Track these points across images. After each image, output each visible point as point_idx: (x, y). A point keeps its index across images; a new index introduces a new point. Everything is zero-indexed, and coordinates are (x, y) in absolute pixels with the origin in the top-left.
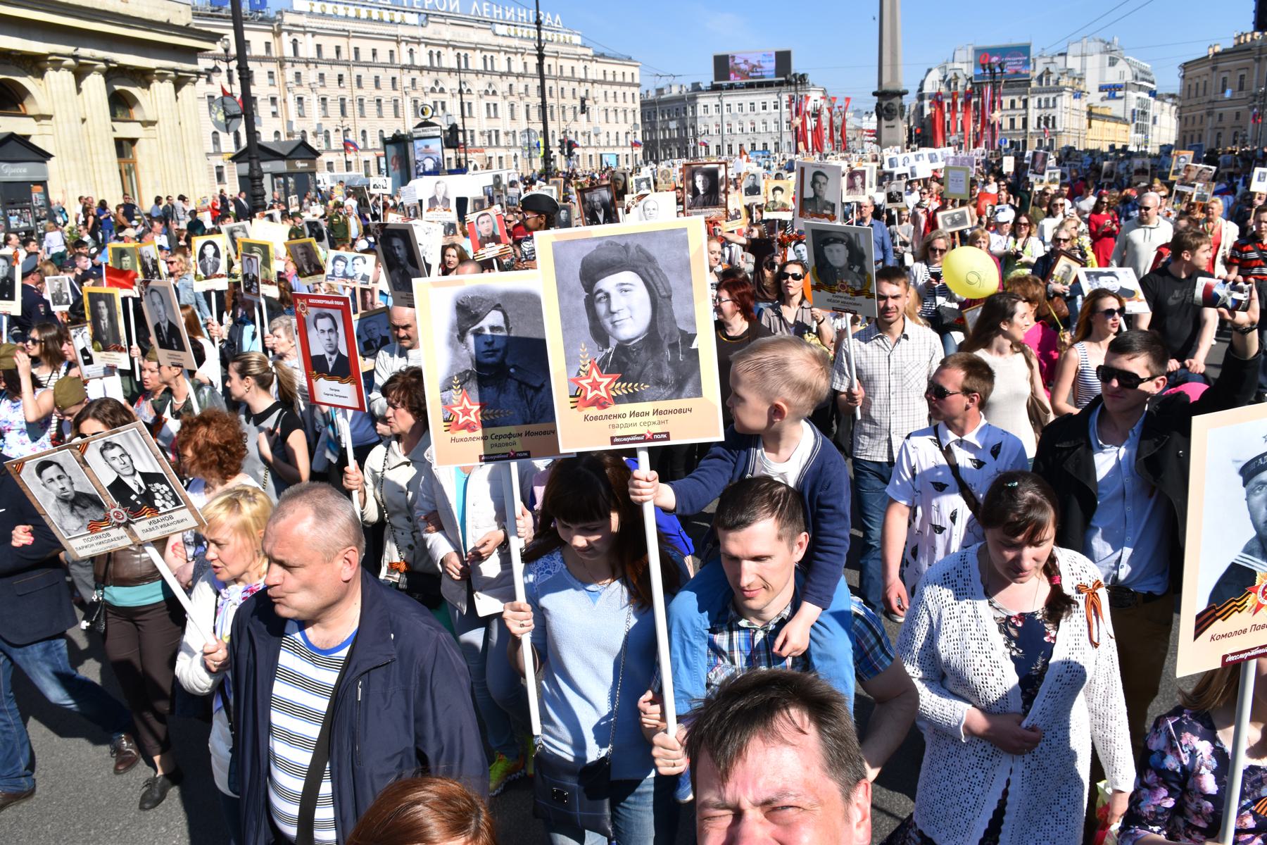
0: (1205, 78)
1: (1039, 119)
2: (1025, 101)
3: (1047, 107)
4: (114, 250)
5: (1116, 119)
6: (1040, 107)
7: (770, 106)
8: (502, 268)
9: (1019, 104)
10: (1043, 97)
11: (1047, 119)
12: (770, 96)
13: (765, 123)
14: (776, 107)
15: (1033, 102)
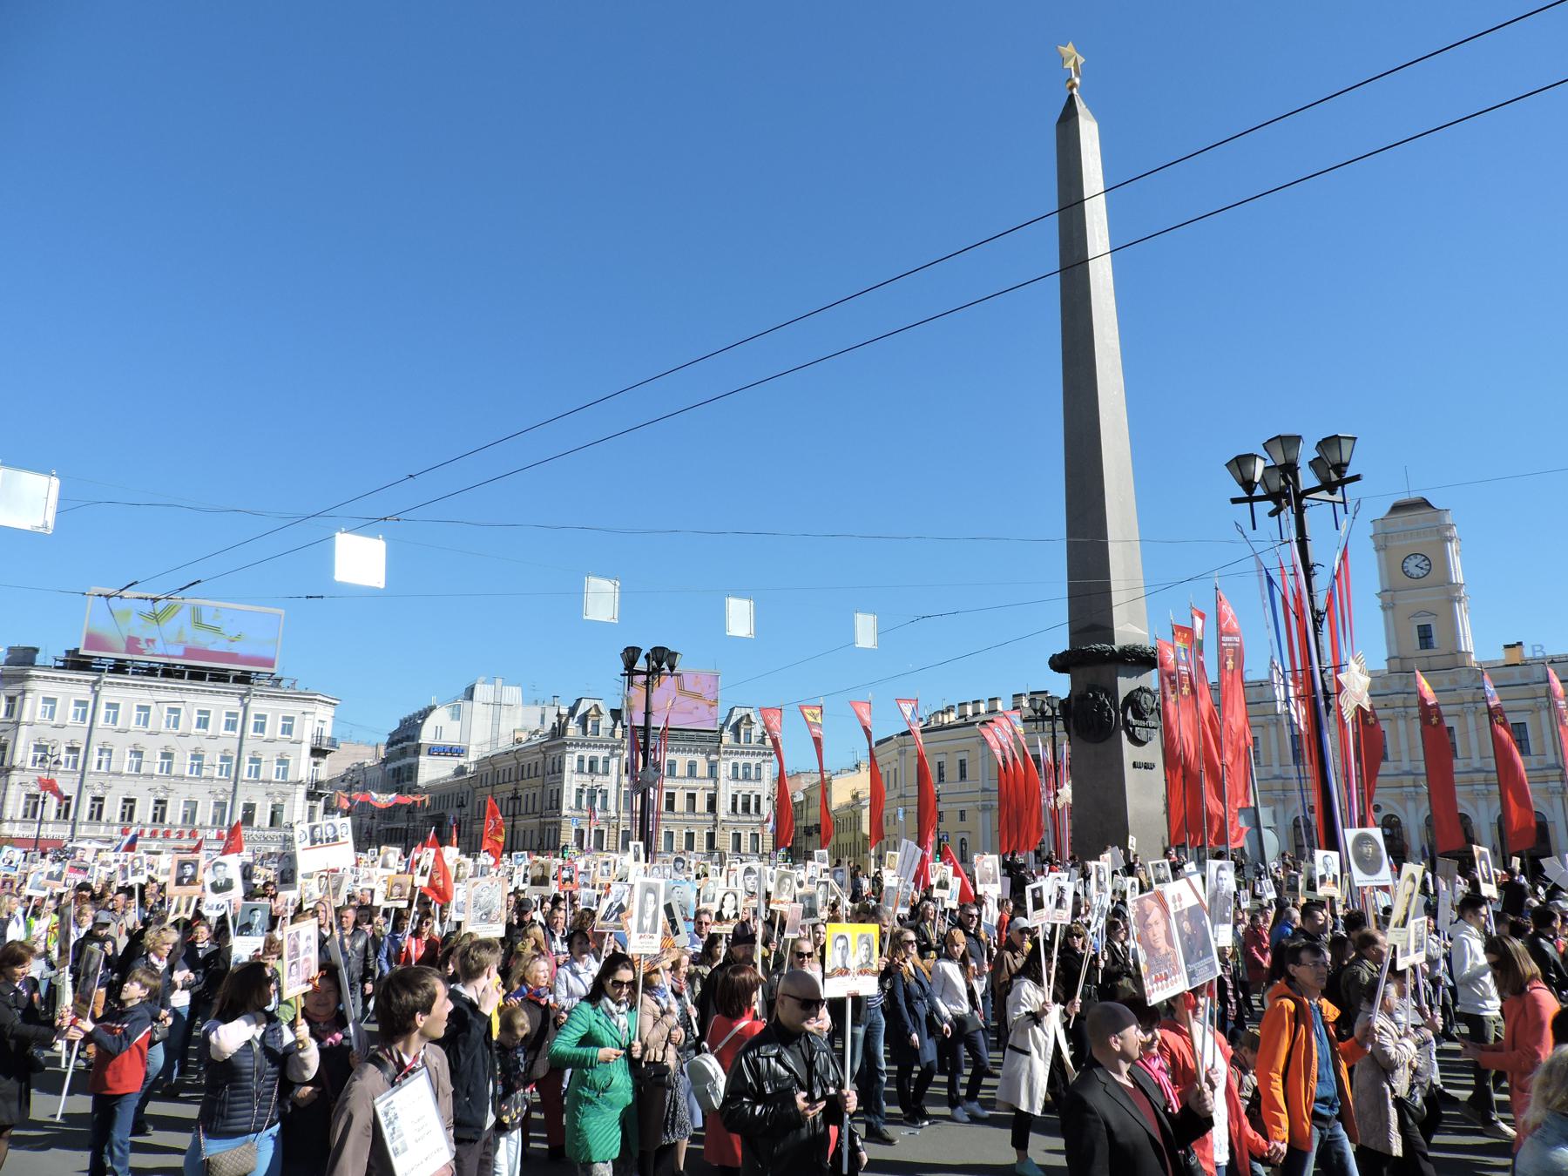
0: (895, 765)
1: (735, 797)
2: (713, 767)
3: (747, 777)
4: (657, 886)
5: (950, 727)
6: (581, 771)
7: (217, 724)
8: (1201, 652)
9: (702, 768)
10: (741, 760)
11: (747, 798)
12: (190, 698)
13: (138, 754)
14: (230, 725)
15: (724, 769)
